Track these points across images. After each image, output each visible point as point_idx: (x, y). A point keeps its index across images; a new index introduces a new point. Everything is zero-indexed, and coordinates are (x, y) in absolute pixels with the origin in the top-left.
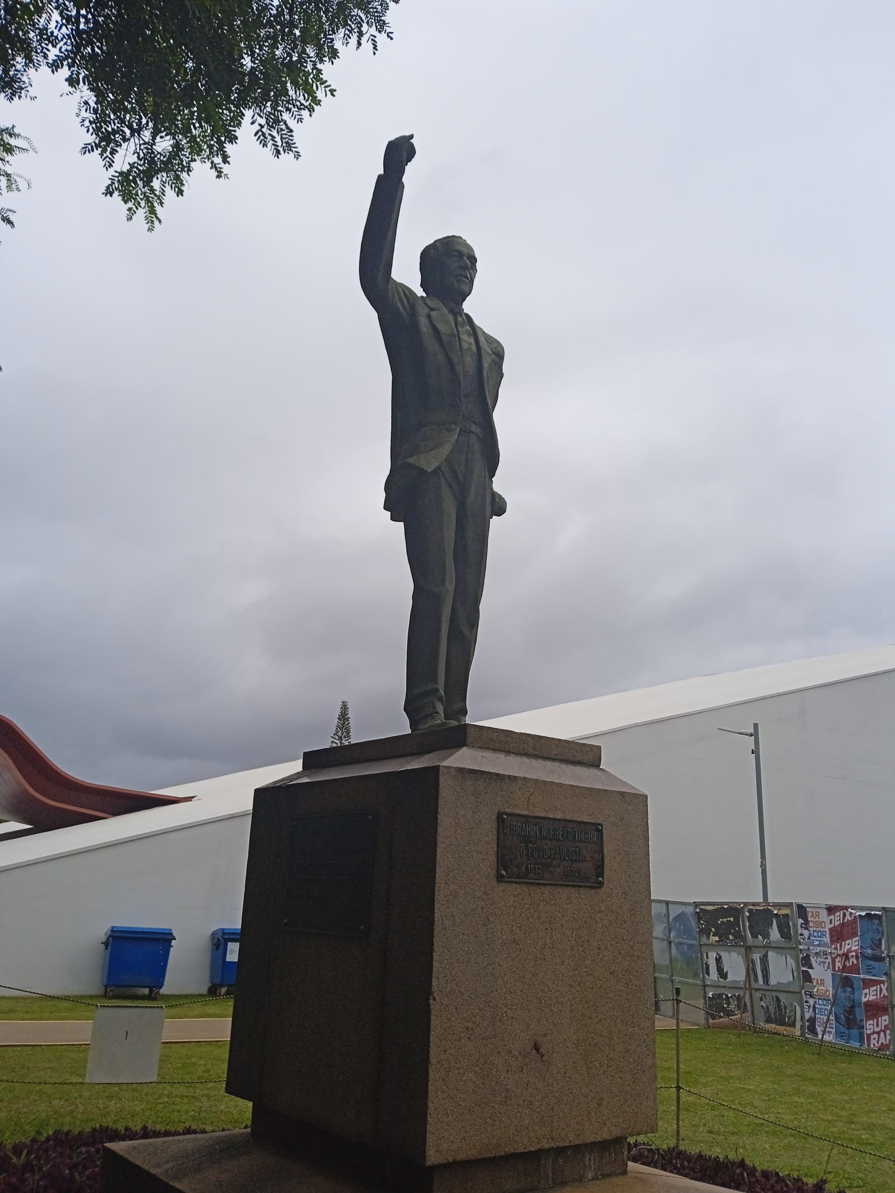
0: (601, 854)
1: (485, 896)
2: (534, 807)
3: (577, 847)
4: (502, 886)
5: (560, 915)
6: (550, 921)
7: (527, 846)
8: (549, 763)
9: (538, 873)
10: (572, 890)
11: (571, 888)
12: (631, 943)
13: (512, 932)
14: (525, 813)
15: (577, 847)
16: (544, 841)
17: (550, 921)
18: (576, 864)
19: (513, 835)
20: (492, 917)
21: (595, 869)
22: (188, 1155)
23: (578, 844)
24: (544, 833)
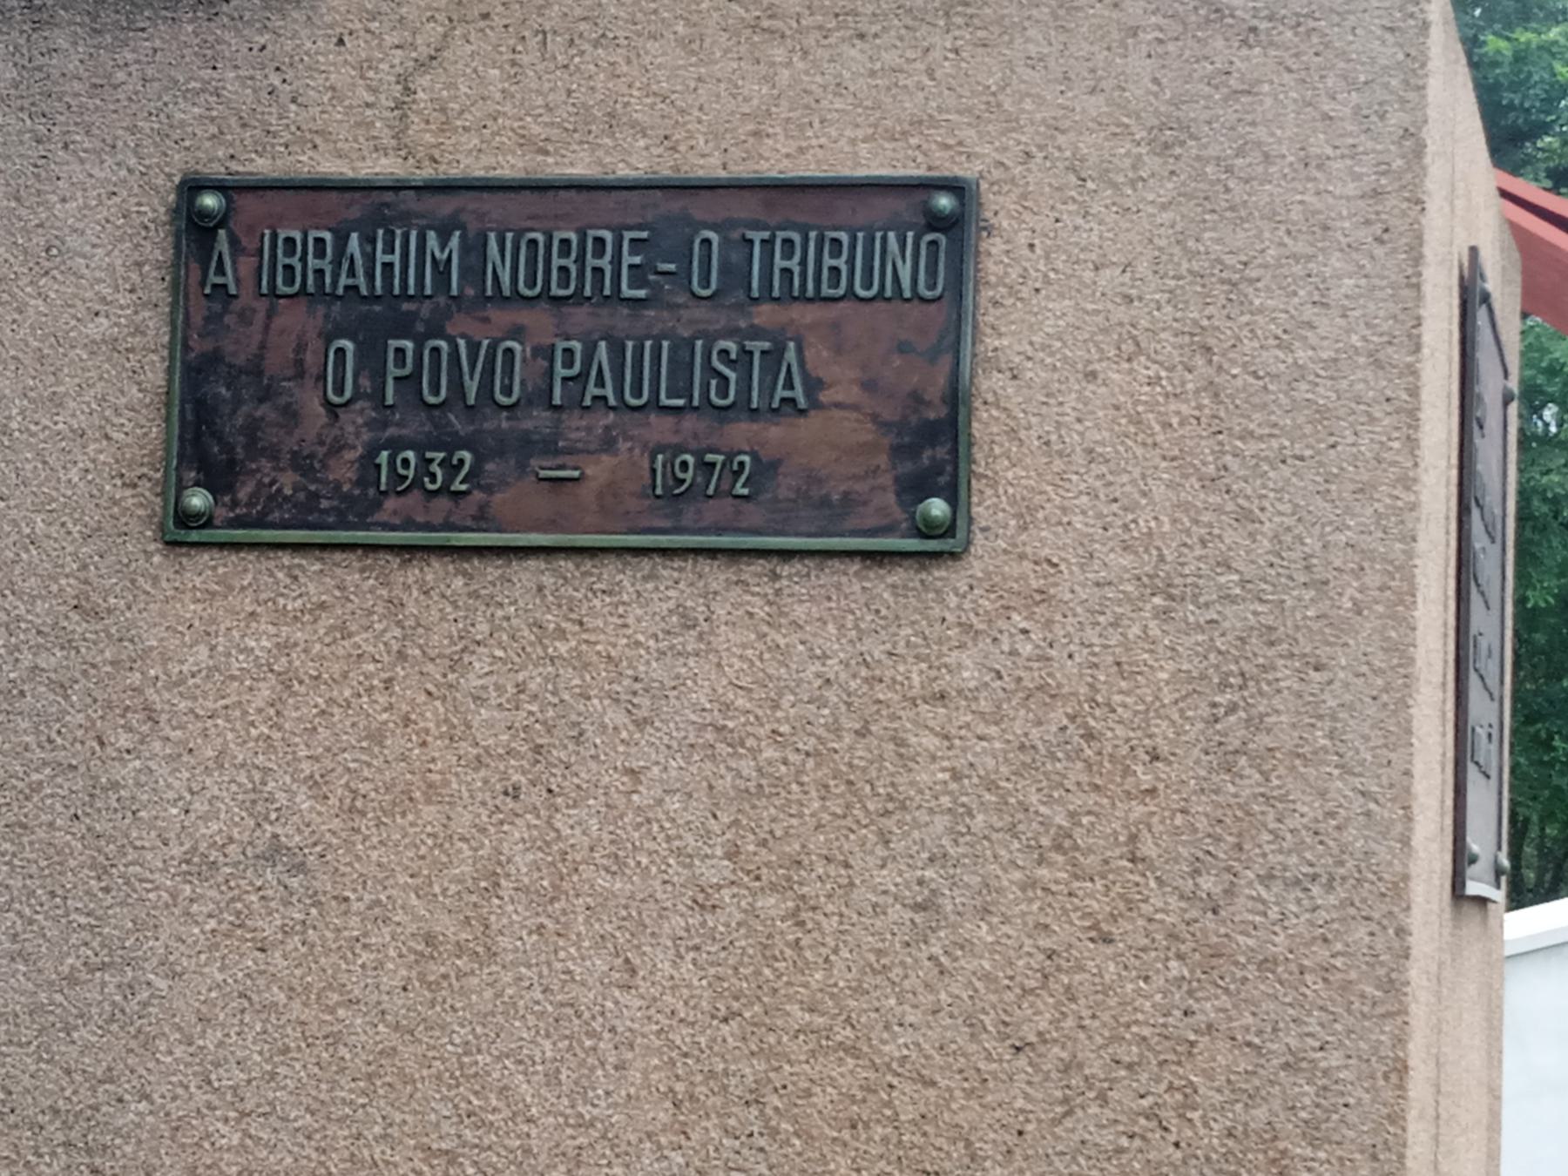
0: (946, 361)
1: (76, 624)
2: (445, 128)
3: (756, 333)
4: (204, 569)
5: (614, 716)
6: (538, 749)
7: (372, 358)
8: (1454, 473)
9: (445, 490)
10: (716, 575)
11: (705, 565)
12: (1207, 883)
13: (257, 804)
14: (386, 167)
15: (756, 333)
16: (502, 317)
17: (538, 749)
18: (740, 432)
19: (273, 293)
20: (129, 729)
21: (898, 452)
22: (1276, 536)
23: (765, 315)
24: (501, 267)
